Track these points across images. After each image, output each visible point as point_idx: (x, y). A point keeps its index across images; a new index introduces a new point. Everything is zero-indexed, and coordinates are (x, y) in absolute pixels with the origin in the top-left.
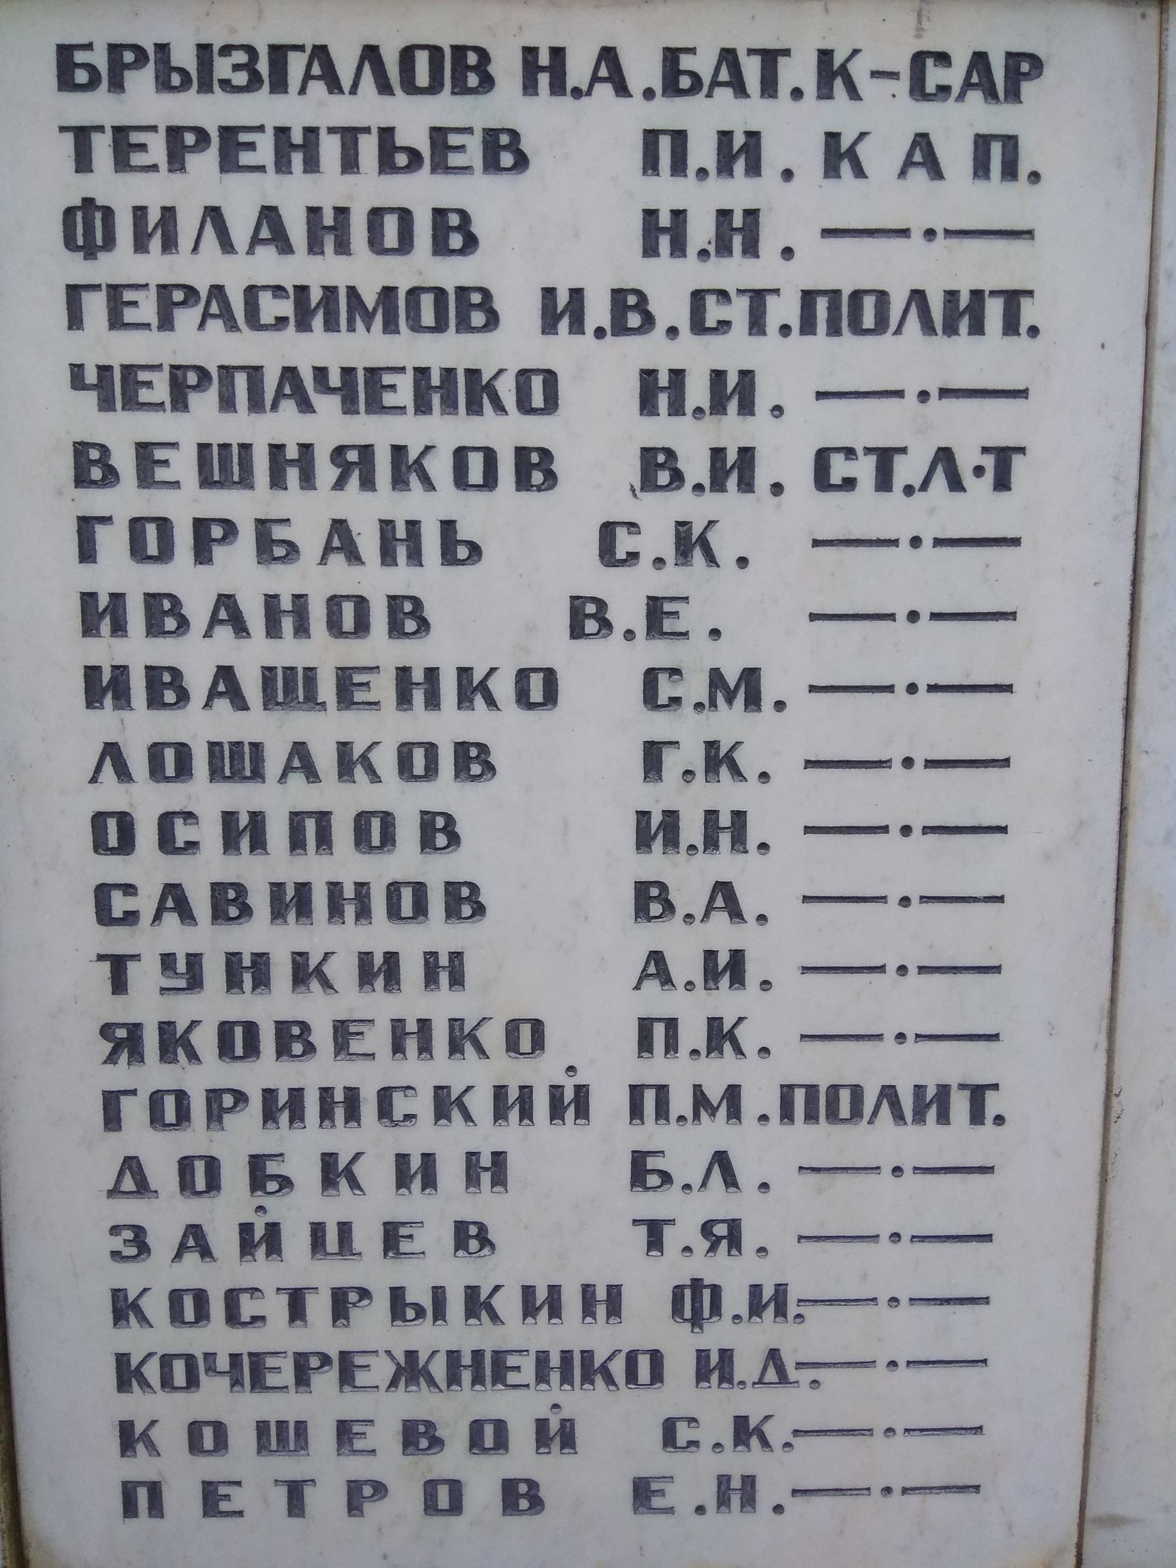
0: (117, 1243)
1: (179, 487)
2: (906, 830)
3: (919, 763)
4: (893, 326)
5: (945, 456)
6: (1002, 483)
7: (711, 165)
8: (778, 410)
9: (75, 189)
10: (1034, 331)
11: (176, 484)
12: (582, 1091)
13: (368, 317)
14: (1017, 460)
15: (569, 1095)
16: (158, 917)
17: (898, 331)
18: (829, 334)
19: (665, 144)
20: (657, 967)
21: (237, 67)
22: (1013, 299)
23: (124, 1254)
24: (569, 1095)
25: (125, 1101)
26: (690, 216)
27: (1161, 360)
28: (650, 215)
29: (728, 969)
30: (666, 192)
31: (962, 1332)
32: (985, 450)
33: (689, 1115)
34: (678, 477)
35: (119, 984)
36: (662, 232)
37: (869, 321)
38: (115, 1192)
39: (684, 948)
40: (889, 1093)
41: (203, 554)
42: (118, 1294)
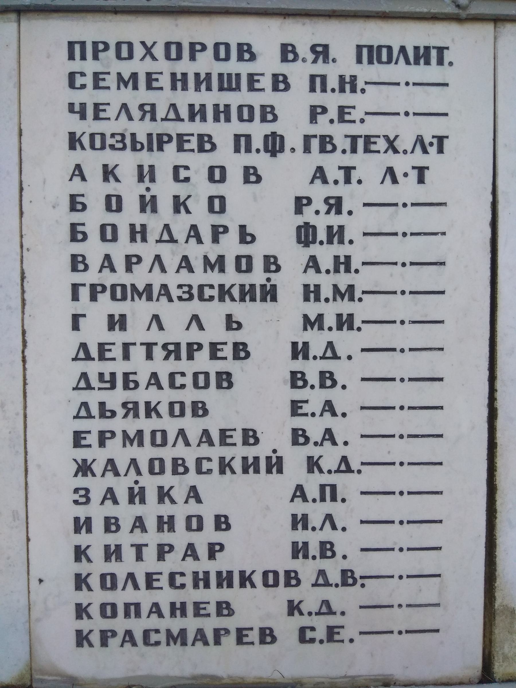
0: (76, 497)
1: (91, 447)
2: (402, 408)
4: (394, 61)
5: (420, 140)
6: (440, 150)
10: (451, 64)
12: (280, 459)
13: (342, 297)
14: (445, 141)
15: (274, 460)
17: (396, 63)
18: (136, 617)
19: (318, 80)
22: (441, 50)
23: (79, 501)
24: (274, 460)
28: (294, 516)
30: (300, 536)
31: (430, 307)
32: (434, 137)
33: (331, 298)
36: (299, 550)
37: (384, 58)
41: (102, 444)
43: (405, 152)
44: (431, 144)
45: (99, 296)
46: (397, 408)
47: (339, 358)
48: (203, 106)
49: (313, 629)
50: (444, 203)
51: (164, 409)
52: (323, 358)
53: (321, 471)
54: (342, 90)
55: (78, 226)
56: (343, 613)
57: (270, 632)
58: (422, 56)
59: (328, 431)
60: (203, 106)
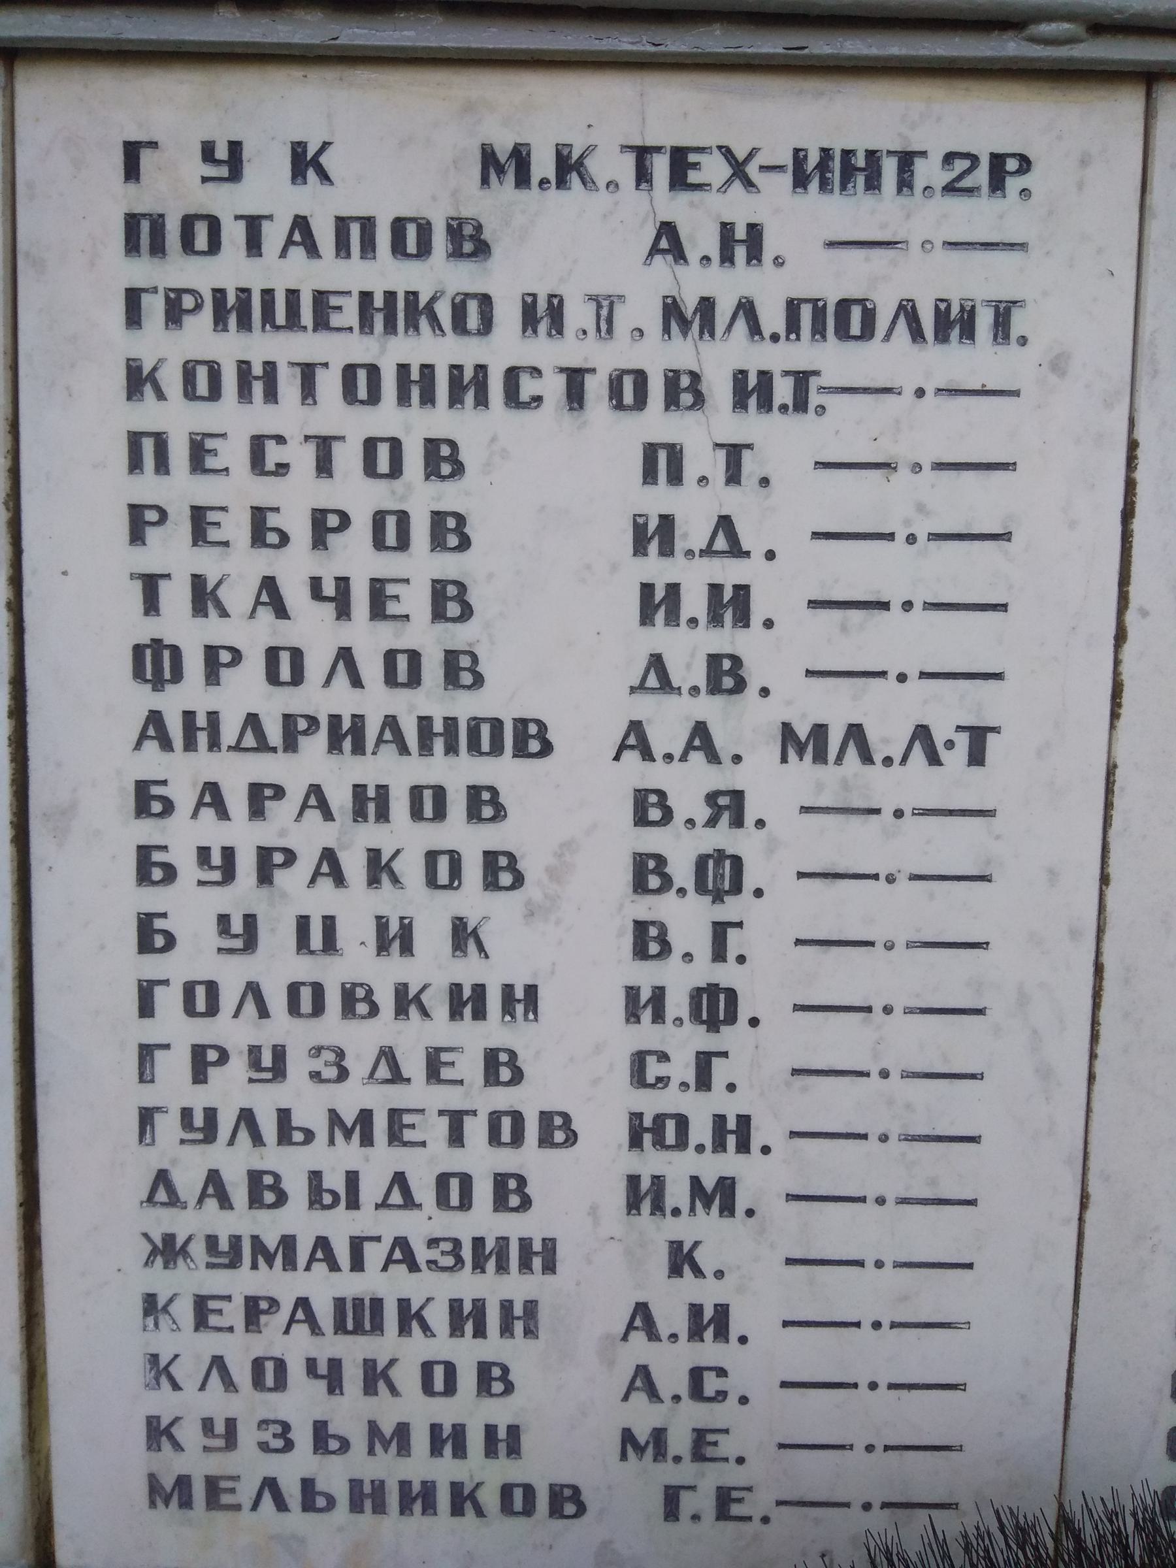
3: (889, 1265)
5: (922, 733)
6: (977, 757)
7: (702, 616)
8: (743, 1340)
9: (146, 630)
11: (231, 1329)
16: (200, 1201)
20: (643, 1380)
21: (275, 1436)
25: (159, 991)
26: (665, 1270)
27: (1154, 229)
29: (732, 605)
32: (960, 728)
34: (667, 882)
35: (151, 605)
38: (640, 688)
39: (681, 849)
40: (908, 311)
42: (152, 1423)
43: (888, 761)
44: (950, 745)
45: (303, 741)
46: (870, 1264)
47: (747, 554)
48: (481, 369)
49: (663, 1057)
50: (1003, 605)
51: (438, 1316)
52: (708, 551)
53: (698, 1272)
54: (727, 258)
55: (226, 175)
56: (740, 1460)
57: (539, 731)
58: (954, 323)
59: (701, 730)
60: (481, 369)
